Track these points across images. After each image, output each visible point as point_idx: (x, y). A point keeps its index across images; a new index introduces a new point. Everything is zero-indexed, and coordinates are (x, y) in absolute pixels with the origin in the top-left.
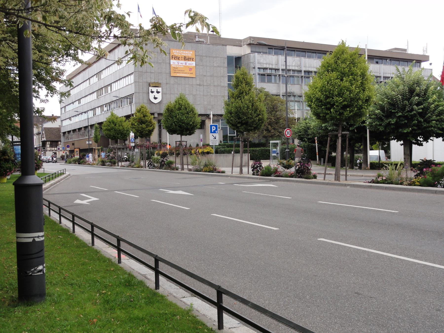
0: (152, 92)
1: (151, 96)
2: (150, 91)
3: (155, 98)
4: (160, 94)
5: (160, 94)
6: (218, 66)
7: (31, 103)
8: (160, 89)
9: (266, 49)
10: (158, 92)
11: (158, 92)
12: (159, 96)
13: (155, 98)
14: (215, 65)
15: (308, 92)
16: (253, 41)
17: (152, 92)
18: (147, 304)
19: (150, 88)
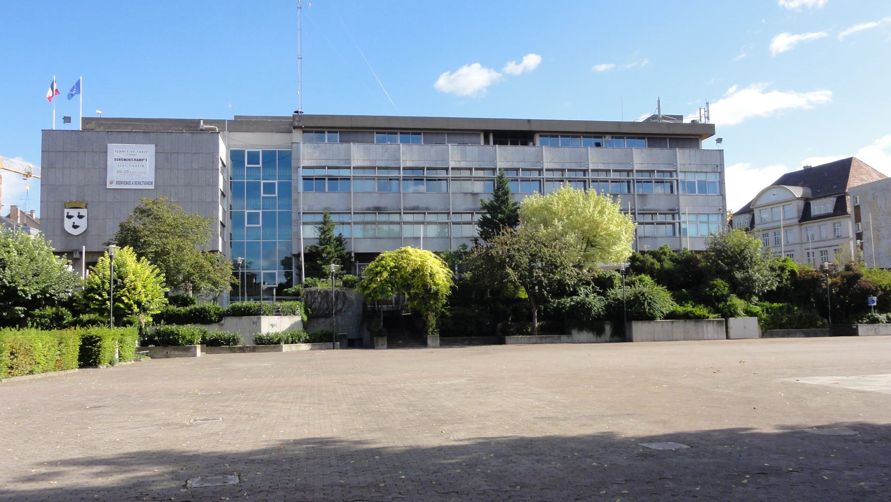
0: (69, 217)
1: (68, 224)
2: (66, 214)
3: (75, 227)
4: (85, 220)
5: (85, 220)
6: (202, 168)
7: (437, 78)
8: (84, 212)
9: (645, 142)
10: (80, 217)
11: (80, 217)
12: (83, 224)
13: (75, 227)
14: (195, 166)
15: (863, 278)
16: (299, 121)
17: (69, 217)
18: (234, 340)
19: (66, 211)
